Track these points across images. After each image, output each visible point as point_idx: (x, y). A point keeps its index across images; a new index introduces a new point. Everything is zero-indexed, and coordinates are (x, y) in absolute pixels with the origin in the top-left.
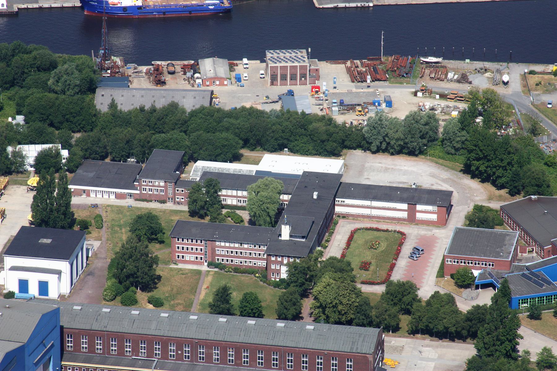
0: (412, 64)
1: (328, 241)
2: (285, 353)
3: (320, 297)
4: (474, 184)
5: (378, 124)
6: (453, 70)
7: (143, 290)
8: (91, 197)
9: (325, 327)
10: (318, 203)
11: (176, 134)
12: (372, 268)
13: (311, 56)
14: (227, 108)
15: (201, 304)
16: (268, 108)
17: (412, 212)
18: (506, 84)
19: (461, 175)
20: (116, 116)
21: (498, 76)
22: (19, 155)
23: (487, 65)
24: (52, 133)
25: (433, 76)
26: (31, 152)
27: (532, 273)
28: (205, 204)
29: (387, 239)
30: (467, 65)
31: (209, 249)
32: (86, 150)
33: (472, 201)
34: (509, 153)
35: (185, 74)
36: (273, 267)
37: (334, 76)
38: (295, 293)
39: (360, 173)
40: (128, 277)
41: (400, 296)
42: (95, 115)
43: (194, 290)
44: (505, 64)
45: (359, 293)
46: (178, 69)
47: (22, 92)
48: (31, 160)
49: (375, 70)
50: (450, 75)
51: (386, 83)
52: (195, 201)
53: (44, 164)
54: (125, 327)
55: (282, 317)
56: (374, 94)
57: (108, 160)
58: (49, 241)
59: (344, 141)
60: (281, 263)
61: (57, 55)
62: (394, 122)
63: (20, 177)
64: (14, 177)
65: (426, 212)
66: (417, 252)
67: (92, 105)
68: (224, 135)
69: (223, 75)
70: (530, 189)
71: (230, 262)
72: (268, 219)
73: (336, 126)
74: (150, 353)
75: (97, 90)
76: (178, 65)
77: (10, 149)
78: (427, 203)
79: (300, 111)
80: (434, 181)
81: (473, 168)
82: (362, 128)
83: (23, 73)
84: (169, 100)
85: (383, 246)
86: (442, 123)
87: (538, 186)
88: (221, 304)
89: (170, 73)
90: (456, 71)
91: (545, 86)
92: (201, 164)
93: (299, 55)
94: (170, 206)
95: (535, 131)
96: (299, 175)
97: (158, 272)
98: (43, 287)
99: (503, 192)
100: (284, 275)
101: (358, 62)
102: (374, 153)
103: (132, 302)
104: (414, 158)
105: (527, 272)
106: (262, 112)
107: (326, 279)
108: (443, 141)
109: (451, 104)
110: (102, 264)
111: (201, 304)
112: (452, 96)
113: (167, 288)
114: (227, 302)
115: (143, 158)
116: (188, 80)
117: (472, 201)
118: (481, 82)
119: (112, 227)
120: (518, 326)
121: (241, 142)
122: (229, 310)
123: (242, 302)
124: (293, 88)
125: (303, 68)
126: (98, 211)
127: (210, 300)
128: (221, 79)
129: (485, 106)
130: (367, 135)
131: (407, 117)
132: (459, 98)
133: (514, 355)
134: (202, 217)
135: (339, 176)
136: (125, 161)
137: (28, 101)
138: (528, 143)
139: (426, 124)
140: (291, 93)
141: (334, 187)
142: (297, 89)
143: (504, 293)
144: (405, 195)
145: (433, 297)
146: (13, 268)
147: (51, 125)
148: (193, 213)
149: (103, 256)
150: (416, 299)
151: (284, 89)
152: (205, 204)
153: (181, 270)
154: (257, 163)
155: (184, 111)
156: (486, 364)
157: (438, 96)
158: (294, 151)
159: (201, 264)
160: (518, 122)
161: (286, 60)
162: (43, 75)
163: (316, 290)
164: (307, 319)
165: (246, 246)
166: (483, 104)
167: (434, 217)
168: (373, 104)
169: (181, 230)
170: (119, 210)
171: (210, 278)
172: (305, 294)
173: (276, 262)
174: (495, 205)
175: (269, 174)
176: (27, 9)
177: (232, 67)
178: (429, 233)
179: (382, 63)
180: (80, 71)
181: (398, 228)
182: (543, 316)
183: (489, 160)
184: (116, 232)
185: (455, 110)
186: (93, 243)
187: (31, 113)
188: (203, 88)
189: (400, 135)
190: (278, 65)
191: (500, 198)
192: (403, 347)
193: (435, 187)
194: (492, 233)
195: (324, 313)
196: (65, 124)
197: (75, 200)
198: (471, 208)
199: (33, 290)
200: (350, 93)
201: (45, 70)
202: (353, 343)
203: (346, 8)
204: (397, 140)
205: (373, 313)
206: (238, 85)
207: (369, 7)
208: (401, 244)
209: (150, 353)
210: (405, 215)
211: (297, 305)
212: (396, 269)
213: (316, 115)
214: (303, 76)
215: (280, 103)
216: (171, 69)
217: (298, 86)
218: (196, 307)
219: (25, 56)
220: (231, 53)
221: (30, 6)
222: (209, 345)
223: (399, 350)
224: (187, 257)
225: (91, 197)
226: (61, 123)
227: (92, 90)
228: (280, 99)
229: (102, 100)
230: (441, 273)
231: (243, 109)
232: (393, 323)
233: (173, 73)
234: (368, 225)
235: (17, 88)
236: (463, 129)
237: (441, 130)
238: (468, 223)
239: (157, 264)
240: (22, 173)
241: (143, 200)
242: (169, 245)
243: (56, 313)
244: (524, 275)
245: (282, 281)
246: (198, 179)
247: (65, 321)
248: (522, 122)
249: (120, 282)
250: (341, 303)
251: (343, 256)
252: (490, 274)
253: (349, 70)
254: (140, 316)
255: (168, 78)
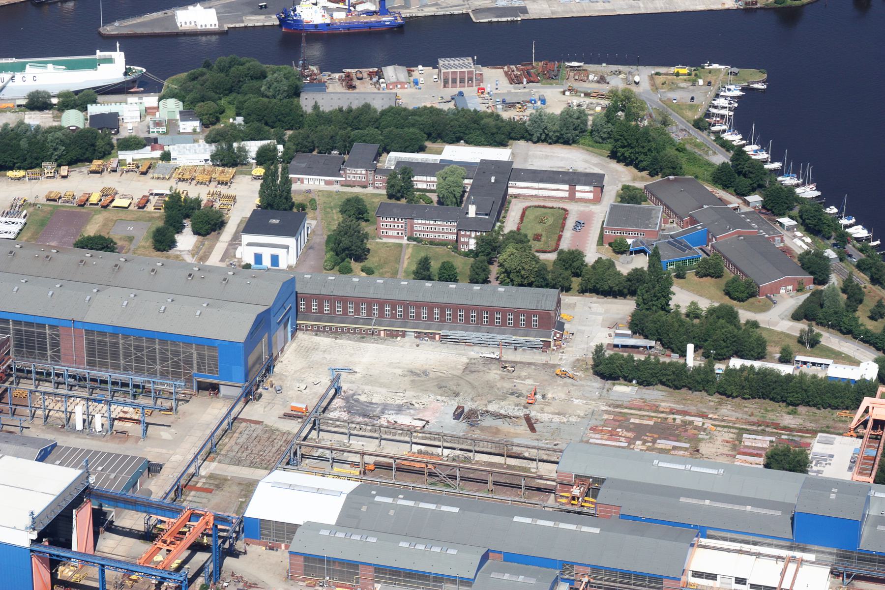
0: (559, 67)
1: (504, 217)
2: (481, 311)
3: (506, 265)
4: (620, 167)
5: (538, 119)
6: (593, 72)
7: (356, 260)
8: (307, 184)
9: (514, 289)
10: (494, 183)
11: (371, 130)
12: (543, 239)
13: (476, 63)
14: (411, 107)
15: (405, 272)
16: (446, 107)
17: (572, 192)
18: (637, 83)
19: (608, 160)
20: (320, 118)
21: (630, 78)
22: (242, 149)
23: (621, 68)
24: (268, 131)
25: (577, 77)
26: (253, 147)
27: (676, 241)
28: (400, 187)
29: (553, 215)
30: (604, 68)
31: (408, 226)
32: (297, 145)
33: (620, 181)
34: (649, 141)
35: (371, 79)
36: (463, 240)
37: (495, 79)
38: (484, 261)
39: (526, 160)
40: (344, 250)
41: (570, 262)
42: (302, 116)
43: (398, 260)
44: (635, 67)
45: (537, 260)
46: (365, 75)
47: (240, 97)
48: (253, 153)
49: (528, 73)
50: (591, 77)
51: (539, 85)
52: (393, 186)
53: (264, 157)
54: (348, 292)
55: (473, 281)
56: (530, 94)
57: (315, 153)
58: (277, 221)
59: (510, 133)
60: (470, 237)
61: (265, 66)
62: (551, 117)
63: (244, 168)
64: (239, 168)
65: (584, 192)
66: (578, 224)
67: (299, 107)
68: (412, 130)
69: (404, 80)
70: (667, 171)
71: (425, 236)
72: (454, 200)
73: (502, 121)
74: (369, 313)
75: (302, 95)
76: (365, 71)
77: (235, 145)
78: (585, 184)
79: (472, 109)
80: (587, 165)
81: (619, 154)
82: (525, 123)
83: (240, 81)
84: (362, 103)
85: (550, 221)
86: (590, 118)
87: (673, 168)
88: (423, 272)
89: (358, 79)
90: (595, 73)
91: (669, 85)
92: (393, 155)
93: (466, 62)
94: (370, 190)
95: (665, 123)
96: (476, 163)
97: (368, 246)
98: (275, 259)
99: (645, 173)
100: (472, 245)
101: (513, 67)
102: (535, 143)
103: (347, 271)
104: (568, 147)
105: (671, 240)
106: (441, 110)
107: (511, 248)
108: (592, 132)
109: (594, 101)
110: (321, 239)
111: (405, 272)
112: (595, 94)
113: (376, 259)
114: (428, 270)
115: (346, 149)
116: (375, 84)
117: (620, 181)
118: (617, 83)
119: (325, 208)
120: (671, 285)
121: (425, 136)
122: (429, 276)
123: (440, 269)
124: (462, 89)
125: (470, 73)
126: (311, 196)
127: (414, 267)
128: (402, 83)
129: (623, 103)
130: (529, 128)
131: (562, 112)
132: (602, 96)
133: (667, 308)
134: (398, 199)
135: (509, 163)
136: (330, 153)
137: (246, 104)
138: (662, 133)
139: (578, 118)
140: (461, 94)
141: (507, 172)
142: (466, 90)
143: (655, 257)
144: (566, 178)
145: (597, 262)
146: (249, 244)
147: (266, 124)
148: (390, 196)
149: (320, 233)
150: (583, 265)
151: (455, 91)
152: (400, 187)
153: (385, 243)
154: (440, 153)
155: (375, 111)
156: (646, 316)
157: (582, 95)
158: (468, 142)
159: (402, 238)
160: (651, 116)
161: (455, 66)
162: (256, 83)
163: (501, 258)
164: (494, 283)
165: (439, 223)
166: (622, 101)
167: (590, 196)
168: (530, 102)
169: (384, 211)
170: (329, 194)
171: (410, 250)
172: (491, 262)
173: (465, 236)
174: (640, 185)
175: (451, 162)
176: (235, 28)
177: (410, 73)
178: (587, 209)
179: (533, 68)
180: (287, 78)
181: (561, 205)
182: (687, 276)
183: (632, 148)
184: (329, 213)
185: (597, 108)
186: (311, 223)
187: (249, 115)
188: (387, 91)
189: (557, 127)
190: (450, 70)
191: (642, 179)
192: (575, 304)
193: (588, 171)
194: (640, 208)
195: (509, 277)
196: (278, 123)
197: (295, 187)
198: (620, 187)
199: (267, 262)
200: (509, 93)
201: (256, 78)
202: (538, 301)
203: (498, 22)
204: (554, 132)
205: (549, 277)
206: (414, 88)
207: (517, 21)
208: (565, 219)
209: (369, 313)
210: (566, 194)
211: (486, 271)
212: (562, 239)
213: (485, 112)
214: (470, 79)
215: (453, 102)
216: (359, 75)
217: (466, 88)
218: (401, 274)
219: (240, 67)
220: (409, 62)
221: (237, 25)
222: (418, 305)
223: (573, 306)
224: (390, 233)
225: (307, 184)
226: (274, 122)
227: (297, 94)
228: (453, 99)
229: (307, 102)
230: (601, 240)
231: (425, 108)
232: (567, 285)
233: (361, 79)
234: (537, 204)
235: (234, 94)
236: (608, 122)
237: (590, 123)
238: (619, 200)
239: (367, 239)
240: (245, 164)
241: (348, 186)
242: (375, 223)
243: (292, 281)
244: (669, 242)
245: (471, 251)
246: (393, 168)
247: (298, 289)
248: (654, 116)
249: (337, 254)
250: (523, 269)
251: (519, 229)
252: (641, 242)
253: (506, 73)
254: (357, 282)
255: (356, 83)
